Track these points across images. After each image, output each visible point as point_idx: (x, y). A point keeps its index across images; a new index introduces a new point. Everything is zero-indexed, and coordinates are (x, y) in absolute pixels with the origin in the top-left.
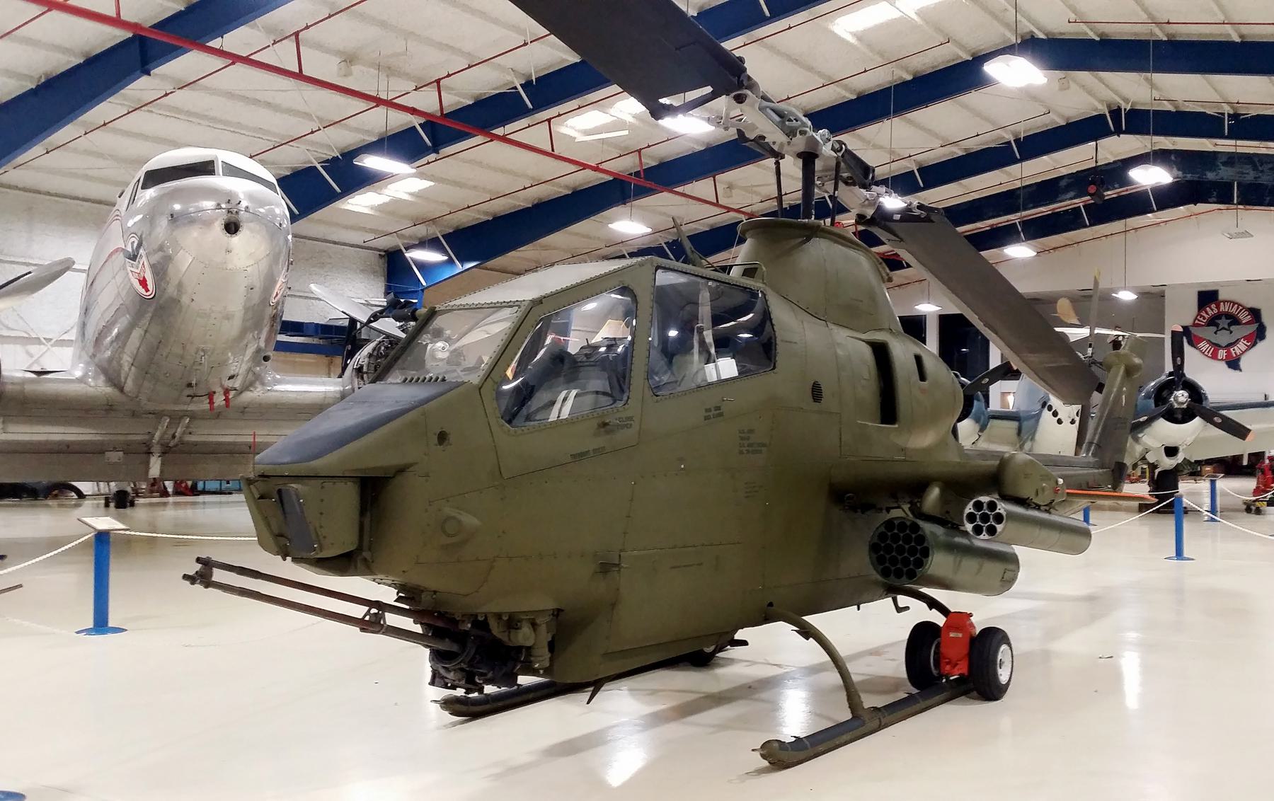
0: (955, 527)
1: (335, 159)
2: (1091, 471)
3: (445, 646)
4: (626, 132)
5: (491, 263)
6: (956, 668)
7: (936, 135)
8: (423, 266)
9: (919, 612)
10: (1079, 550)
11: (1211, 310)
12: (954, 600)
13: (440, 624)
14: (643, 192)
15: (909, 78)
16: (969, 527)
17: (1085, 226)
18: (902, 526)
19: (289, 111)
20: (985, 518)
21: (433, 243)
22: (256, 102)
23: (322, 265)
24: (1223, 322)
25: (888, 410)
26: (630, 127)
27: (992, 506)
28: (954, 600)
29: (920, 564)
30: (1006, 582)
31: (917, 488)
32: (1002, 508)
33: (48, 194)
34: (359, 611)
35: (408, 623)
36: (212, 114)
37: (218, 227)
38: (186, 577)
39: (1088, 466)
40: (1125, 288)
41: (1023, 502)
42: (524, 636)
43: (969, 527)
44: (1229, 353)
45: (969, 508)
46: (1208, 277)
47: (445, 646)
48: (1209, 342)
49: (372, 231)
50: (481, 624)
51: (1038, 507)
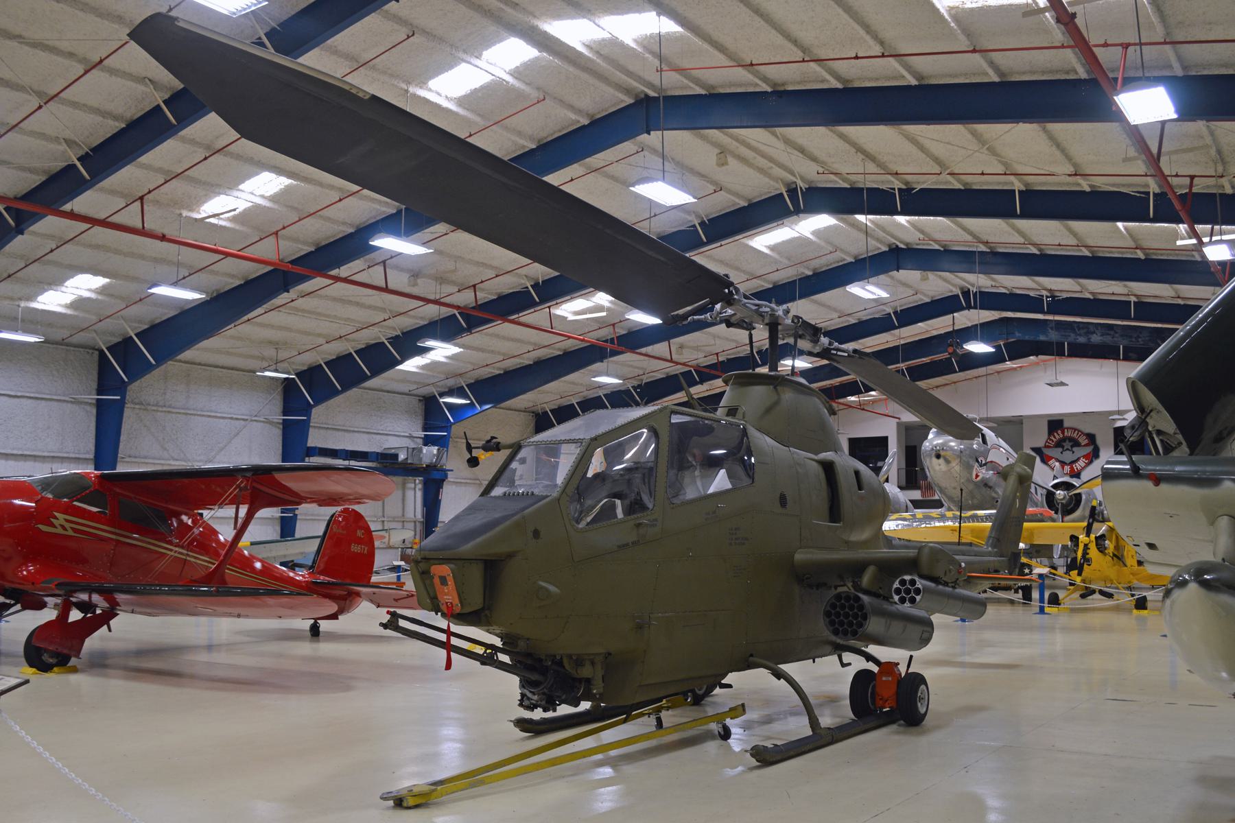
0: (888, 598)
1: (397, 336)
2: (992, 558)
3: (534, 677)
4: (604, 314)
5: (503, 405)
6: (890, 703)
7: (835, 310)
8: (451, 407)
9: (858, 663)
11: (1058, 436)
12: (883, 653)
13: (529, 662)
14: (614, 353)
15: (810, 273)
16: (896, 598)
17: (336, 393)
18: (848, 598)
19: (370, 307)
20: (908, 591)
21: (459, 392)
22: (350, 302)
24: (1067, 445)
25: (834, 512)
26: (608, 310)
27: (913, 582)
28: (883, 653)
29: (861, 625)
30: (925, 641)
31: (858, 568)
32: (920, 583)
33: (200, 364)
34: (480, 650)
35: (504, 658)
36: (319, 310)
38: (382, 625)
39: (989, 554)
41: (936, 580)
42: (586, 672)
43: (896, 598)
44: (1072, 468)
45: (896, 585)
47: (534, 677)
48: (1058, 460)
49: (415, 383)
51: (946, 584)
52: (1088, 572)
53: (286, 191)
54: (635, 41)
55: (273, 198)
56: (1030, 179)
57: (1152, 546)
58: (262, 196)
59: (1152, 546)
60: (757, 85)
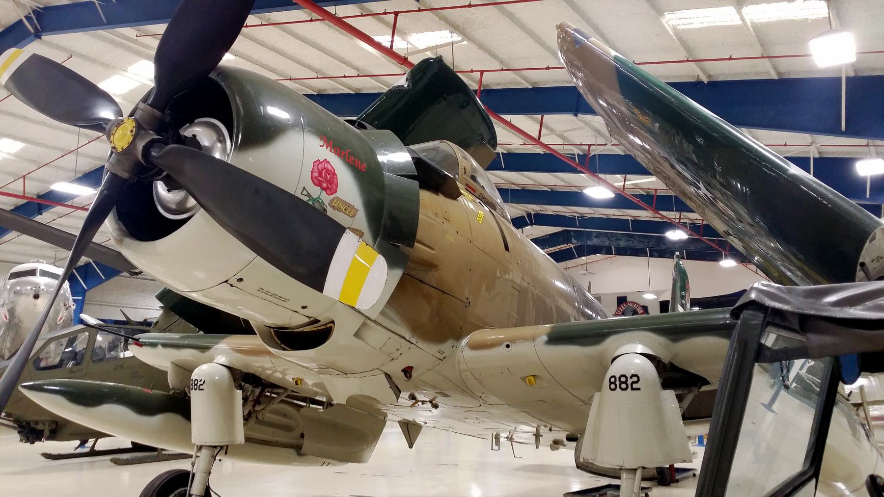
10: (876, 473)
23: (143, 291)
37: (31, 296)
40: (650, 292)
42: (40, 427)
46: (622, 290)
50: (28, 423)
52: (561, 411)
53: (23, 150)
54: (752, 23)
55: (16, 155)
56: (824, 149)
57: (304, 307)
58: (9, 153)
59: (304, 307)
60: (521, 83)
